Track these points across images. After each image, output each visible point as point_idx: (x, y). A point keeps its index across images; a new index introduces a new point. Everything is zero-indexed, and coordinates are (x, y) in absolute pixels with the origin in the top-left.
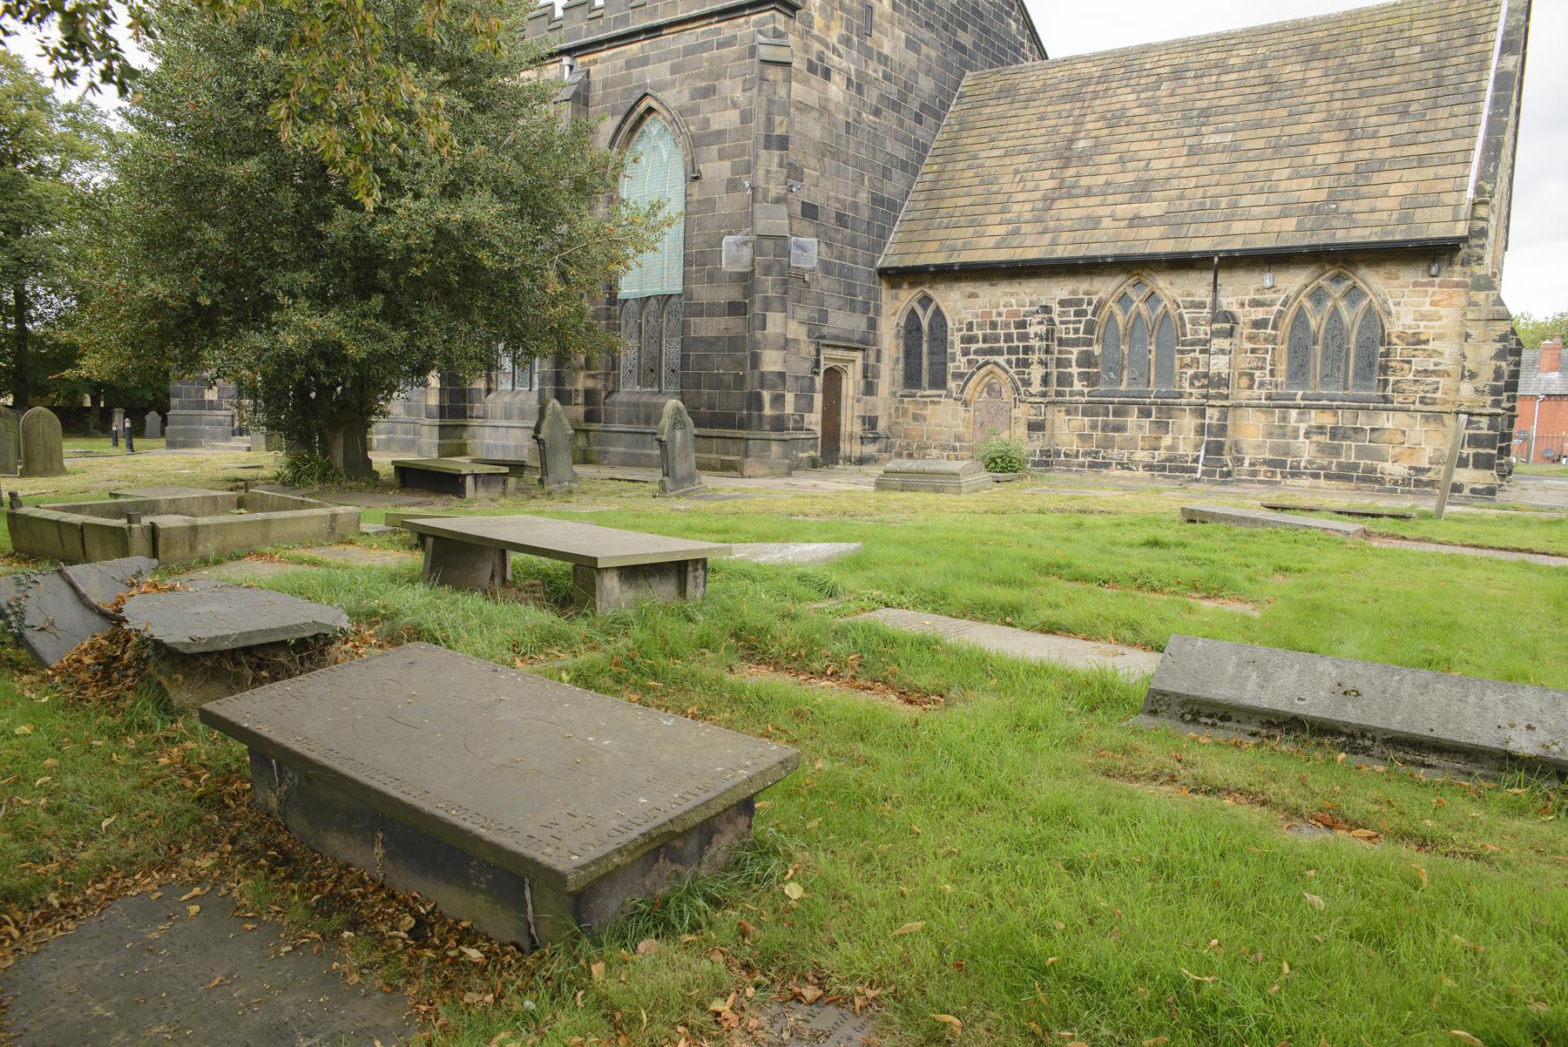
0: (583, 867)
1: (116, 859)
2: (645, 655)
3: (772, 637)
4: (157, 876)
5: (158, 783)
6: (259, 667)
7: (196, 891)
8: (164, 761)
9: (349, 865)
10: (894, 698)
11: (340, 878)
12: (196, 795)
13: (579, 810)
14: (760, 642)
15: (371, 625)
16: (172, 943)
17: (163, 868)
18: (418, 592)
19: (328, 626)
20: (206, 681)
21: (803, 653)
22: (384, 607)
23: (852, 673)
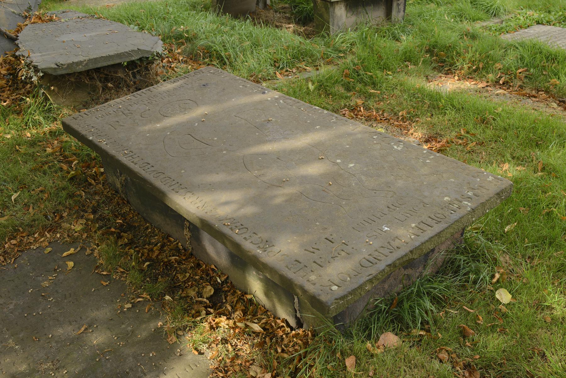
0: (343, 298)
1: (22, 223)
2: (366, 69)
3: (457, 53)
4: (48, 236)
5: (46, 167)
6: (107, 80)
7: (72, 250)
8: (49, 150)
9: (169, 236)
10: (555, 105)
11: (163, 246)
12: (69, 176)
13: (334, 235)
14: (448, 57)
15: (179, 45)
16: (57, 291)
17: (52, 229)
18: (208, 19)
19: (148, 52)
20: (74, 90)
21: (481, 66)
22: (187, 32)
23: (520, 83)
